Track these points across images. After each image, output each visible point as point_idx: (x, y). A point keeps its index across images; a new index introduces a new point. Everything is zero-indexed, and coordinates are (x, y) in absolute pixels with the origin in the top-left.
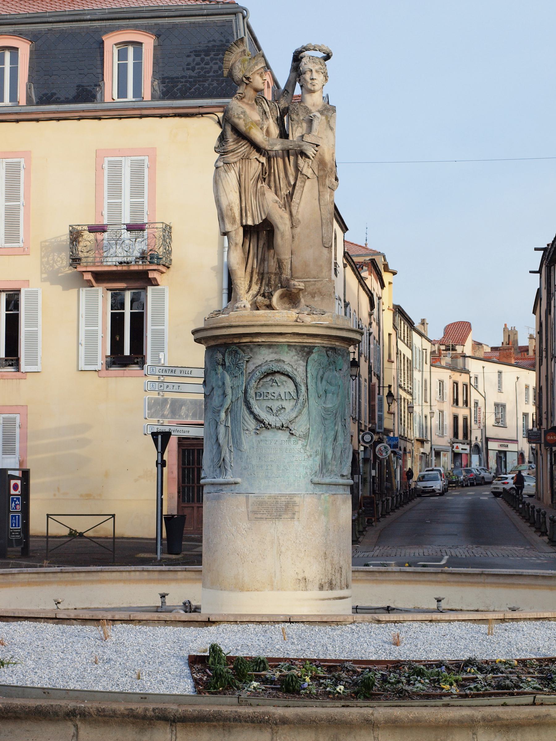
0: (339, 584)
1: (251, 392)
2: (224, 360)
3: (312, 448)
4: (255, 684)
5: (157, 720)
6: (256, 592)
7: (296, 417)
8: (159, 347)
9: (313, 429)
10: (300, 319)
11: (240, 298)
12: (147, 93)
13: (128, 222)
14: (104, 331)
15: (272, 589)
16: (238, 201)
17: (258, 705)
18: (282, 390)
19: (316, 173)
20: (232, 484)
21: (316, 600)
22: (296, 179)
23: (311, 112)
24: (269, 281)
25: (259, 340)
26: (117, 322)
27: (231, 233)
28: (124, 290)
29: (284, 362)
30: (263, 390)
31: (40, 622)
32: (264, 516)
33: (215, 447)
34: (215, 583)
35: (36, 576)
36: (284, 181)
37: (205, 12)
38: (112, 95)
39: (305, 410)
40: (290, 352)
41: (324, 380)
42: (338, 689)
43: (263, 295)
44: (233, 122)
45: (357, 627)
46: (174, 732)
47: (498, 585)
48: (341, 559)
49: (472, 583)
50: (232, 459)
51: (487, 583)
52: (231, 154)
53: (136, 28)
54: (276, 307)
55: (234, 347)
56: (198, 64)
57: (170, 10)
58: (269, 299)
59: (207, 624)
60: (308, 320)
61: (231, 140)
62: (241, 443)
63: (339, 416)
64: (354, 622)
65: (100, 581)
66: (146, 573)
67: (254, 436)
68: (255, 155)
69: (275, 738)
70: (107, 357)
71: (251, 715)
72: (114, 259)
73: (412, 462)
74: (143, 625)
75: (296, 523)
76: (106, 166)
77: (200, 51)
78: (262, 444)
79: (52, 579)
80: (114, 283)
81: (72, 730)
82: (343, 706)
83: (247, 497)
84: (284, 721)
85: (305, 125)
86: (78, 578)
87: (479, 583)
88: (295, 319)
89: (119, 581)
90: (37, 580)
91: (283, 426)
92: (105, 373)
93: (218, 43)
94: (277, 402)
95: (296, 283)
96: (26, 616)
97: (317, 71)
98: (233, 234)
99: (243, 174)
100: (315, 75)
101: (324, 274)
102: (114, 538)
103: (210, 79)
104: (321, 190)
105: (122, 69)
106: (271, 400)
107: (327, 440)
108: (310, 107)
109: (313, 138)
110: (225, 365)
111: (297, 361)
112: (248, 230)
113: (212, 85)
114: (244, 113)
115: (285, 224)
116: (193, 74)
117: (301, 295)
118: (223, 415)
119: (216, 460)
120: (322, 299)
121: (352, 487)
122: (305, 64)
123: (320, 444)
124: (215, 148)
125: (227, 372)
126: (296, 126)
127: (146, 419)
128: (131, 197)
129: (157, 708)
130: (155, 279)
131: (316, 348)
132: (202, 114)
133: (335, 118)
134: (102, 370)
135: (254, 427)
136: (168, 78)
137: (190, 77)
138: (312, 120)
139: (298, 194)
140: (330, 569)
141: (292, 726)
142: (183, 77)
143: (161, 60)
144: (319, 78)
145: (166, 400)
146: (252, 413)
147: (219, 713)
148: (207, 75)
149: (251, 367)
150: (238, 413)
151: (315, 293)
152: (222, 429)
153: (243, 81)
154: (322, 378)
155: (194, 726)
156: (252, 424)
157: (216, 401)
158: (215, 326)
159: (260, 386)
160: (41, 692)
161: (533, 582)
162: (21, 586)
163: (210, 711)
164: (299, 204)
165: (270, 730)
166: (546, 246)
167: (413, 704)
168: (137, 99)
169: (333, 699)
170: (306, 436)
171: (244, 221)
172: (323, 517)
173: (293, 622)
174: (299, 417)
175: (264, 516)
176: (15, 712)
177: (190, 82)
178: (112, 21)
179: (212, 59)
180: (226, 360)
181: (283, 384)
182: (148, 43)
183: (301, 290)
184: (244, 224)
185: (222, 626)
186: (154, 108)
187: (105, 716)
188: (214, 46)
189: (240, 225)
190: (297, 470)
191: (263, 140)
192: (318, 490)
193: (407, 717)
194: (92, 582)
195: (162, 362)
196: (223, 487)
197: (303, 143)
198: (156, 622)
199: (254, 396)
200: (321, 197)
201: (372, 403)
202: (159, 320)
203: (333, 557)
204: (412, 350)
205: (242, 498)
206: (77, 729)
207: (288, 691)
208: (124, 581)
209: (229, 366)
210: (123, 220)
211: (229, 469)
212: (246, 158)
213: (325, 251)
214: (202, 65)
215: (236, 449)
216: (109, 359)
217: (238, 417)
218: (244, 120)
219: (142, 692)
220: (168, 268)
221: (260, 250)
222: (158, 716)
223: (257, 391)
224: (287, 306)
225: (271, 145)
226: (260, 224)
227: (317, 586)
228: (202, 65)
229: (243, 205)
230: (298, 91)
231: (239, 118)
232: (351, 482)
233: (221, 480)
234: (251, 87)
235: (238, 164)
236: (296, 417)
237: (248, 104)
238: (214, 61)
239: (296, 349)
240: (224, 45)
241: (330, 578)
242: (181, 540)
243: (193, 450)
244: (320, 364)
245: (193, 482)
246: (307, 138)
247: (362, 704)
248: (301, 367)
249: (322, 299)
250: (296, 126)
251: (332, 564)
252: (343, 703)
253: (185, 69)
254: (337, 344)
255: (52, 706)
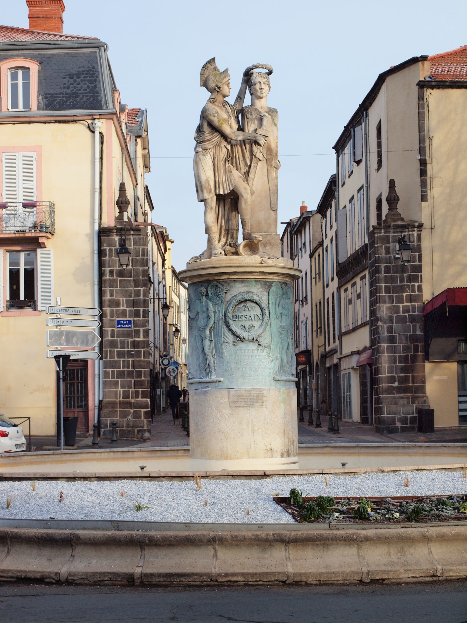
0: (293, 453)
1: (230, 315)
2: (207, 292)
3: (273, 355)
4: (337, 515)
5: (276, 542)
6: (237, 460)
7: (263, 332)
8: (47, 297)
9: (274, 342)
10: (264, 262)
11: (214, 247)
12: (34, 105)
13: (22, 201)
14: (5, 283)
15: (249, 458)
16: (213, 177)
17: (343, 529)
18: (252, 313)
19: (265, 157)
20: (216, 382)
21: (279, 464)
22: (251, 161)
23: (260, 113)
24: (232, 235)
25: (235, 277)
26: (14, 275)
27: (208, 200)
28: (18, 251)
29: (253, 293)
30: (238, 314)
31: (136, 480)
32: (242, 405)
33: (201, 356)
34: (206, 455)
35: (35, 457)
36: (243, 162)
37: (76, 45)
38: (7, 107)
39: (268, 328)
40: (257, 285)
41: (280, 306)
42: (395, 516)
43: (230, 245)
44: (210, 119)
45: (369, 476)
46: (288, 550)
47: (369, 454)
48: (294, 434)
49: (349, 453)
50: (216, 364)
51: (361, 453)
52: (207, 143)
53: (24, 56)
54: (242, 253)
55: (215, 283)
56: (72, 84)
57: (50, 44)
58: (234, 248)
59: (263, 477)
60: (271, 262)
61: (207, 132)
62: (223, 352)
63: (289, 331)
64: (366, 472)
65: (81, 460)
66: (112, 454)
67: (232, 346)
68: (224, 143)
69: (360, 552)
70: (7, 301)
71: (344, 536)
72: (14, 228)
73: (181, 380)
74: (217, 479)
75: (265, 409)
76: (4, 159)
77: (73, 75)
78: (238, 353)
79: (47, 460)
80: (11, 246)
81: (212, 552)
82: (402, 527)
83: (229, 392)
84: (367, 539)
85: (256, 122)
86: (65, 459)
87: (354, 453)
88: (260, 261)
89: (94, 460)
90: (37, 460)
91: (253, 339)
92: (6, 313)
93: (86, 69)
94: (248, 322)
95: (257, 236)
96: (126, 476)
97: (264, 83)
98: (209, 201)
99: (217, 157)
100: (263, 86)
101: (272, 230)
102: (30, 436)
103: (81, 95)
104: (269, 169)
105: (14, 88)
106: (244, 321)
107: (283, 349)
108: (260, 110)
109: (264, 131)
110: (208, 295)
111: (262, 292)
112: (220, 198)
113: (83, 99)
114: (217, 112)
115: (248, 193)
116: (68, 91)
117: (260, 244)
118: (207, 332)
119: (202, 365)
120: (272, 248)
121: (296, 382)
122: (256, 78)
123: (278, 352)
124: (195, 138)
125: (210, 301)
126: (251, 122)
127: (48, 346)
128: (24, 182)
129: (276, 534)
130: (44, 243)
131: (274, 283)
132: (76, 121)
133: (278, 117)
134: (4, 311)
135: (232, 341)
136: (49, 94)
137: (66, 94)
138: (262, 118)
139: (252, 172)
140: (287, 442)
141: (372, 542)
142: (60, 94)
143: (43, 81)
144: (265, 88)
145: (62, 331)
146: (230, 330)
147: (321, 535)
148: (79, 92)
149: (229, 297)
150: (220, 331)
151: (266, 244)
152: (207, 343)
153: (215, 89)
154: (279, 305)
155: (302, 545)
156: (231, 338)
157: (201, 322)
158: (201, 267)
159: (236, 310)
160: (183, 525)
161: (395, 451)
162: (26, 465)
163: (314, 534)
164: (253, 179)
165: (356, 546)
166: (289, 221)
167: (449, 524)
168: (26, 110)
169: (394, 522)
170: (269, 346)
171: (217, 191)
172: (282, 404)
173: (324, 474)
174: (264, 333)
175: (242, 405)
176: (170, 541)
177: (66, 97)
178: (5, 51)
179: (82, 81)
180: (209, 292)
181: (252, 309)
182: (34, 68)
183: (260, 241)
184: (218, 193)
185: (275, 478)
186: (40, 116)
187: (238, 540)
188: (83, 71)
189: (214, 194)
190: (264, 371)
191: (230, 133)
192: (278, 385)
193: (451, 533)
194: (75, 461)
195: (59, 304)
196: (209, 385)
197: (256, 135)
198: (226, 477)
199: (232, 318)
200: (269, 174)
201: (165, 337)
202: (47, 274)
203: (289, 433)
204: (179, 299)
205: (225, 392)
206: (216, 551)
207: (361, 518)
208: (97, 460)
209: (211, 297)
210: (17, 199)
211: (213, 371)
212: (218, 145)
213: (273, 213)
214: (75, 85)
215: (219, 356)
216: (8, 303)
217: (220, 334)
218: (218, 118)
219: (258, 523)
220: (53, 235)
221: (226, 213)
222: (277, 539)
223: (234, 314)
224: (249, 253)
225: (236, 136)
226: (228, 194)
227: (279, 455)
228: (75, 85)
229: (217, 180)
230: (247, 101)
231: (214, 116)
232: (296, 379)
233: (207, 379)
234: (221, 94)
235: (213, 150)
236: (263, 332)
237: (218, 106)
238: (84, 82)
239: (261, 284)
240: (91, 70)
241: (287, 448)
242: (75, 437)
243: (74, 370)
244: (277, 294)
245: (74, 393)
246: (259, 131)
247: (415, 526)
248: (265, 296)
249: (272, 248)
250: (251, 122)
251: (289, 439)
252: (402, 525)
253: (62, 88)
254: (287, 279)
255: (197, 535)
